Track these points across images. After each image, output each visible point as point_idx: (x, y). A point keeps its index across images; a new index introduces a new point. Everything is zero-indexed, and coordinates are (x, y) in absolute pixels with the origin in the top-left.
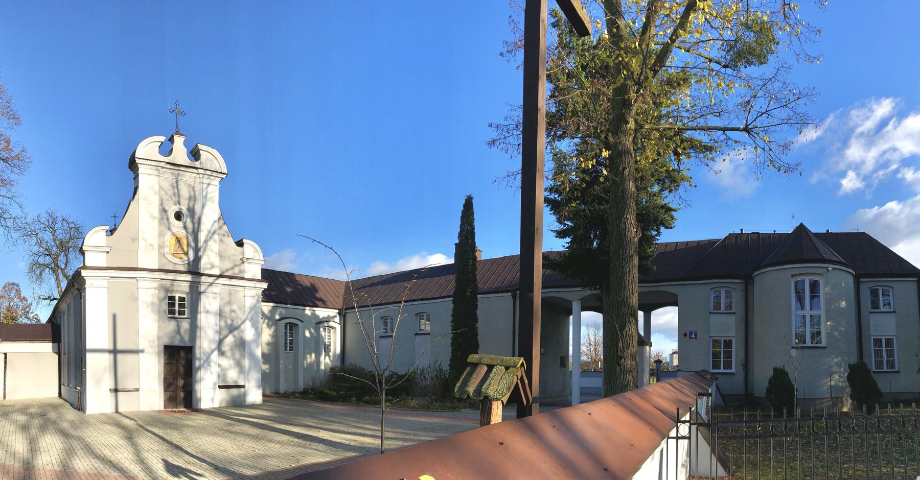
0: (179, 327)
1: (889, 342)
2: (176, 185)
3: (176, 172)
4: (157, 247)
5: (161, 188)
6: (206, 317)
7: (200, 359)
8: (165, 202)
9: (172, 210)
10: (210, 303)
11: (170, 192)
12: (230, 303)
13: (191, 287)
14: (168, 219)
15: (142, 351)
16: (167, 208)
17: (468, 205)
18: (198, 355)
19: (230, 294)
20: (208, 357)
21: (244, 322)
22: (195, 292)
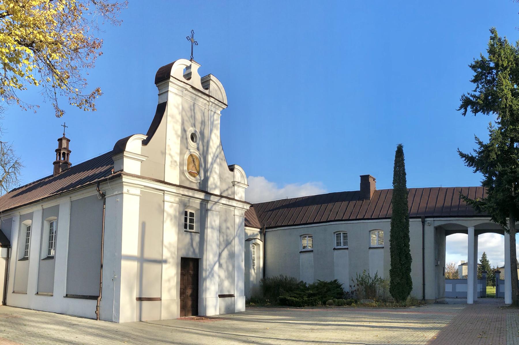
0: (192, 240)
1: (192, 214)
2: (193, 108)
3: (194, 96)
4: (178, 164)
5: (183, 108)
6: (212, 233)
7: (206, 271)
8: (185, 123)
9: (190, 130)
10: (213, 220)
11: (189, 114)
12: (226, 221)
13: (201, 204)
14: (187, 139)
15: (165, 262)
16: (186, 128)
17: (400, 152)
18: (204, 267)
19: (226, 211)
20: (212, 269)
21: (234, 238)
22: (204, 211)
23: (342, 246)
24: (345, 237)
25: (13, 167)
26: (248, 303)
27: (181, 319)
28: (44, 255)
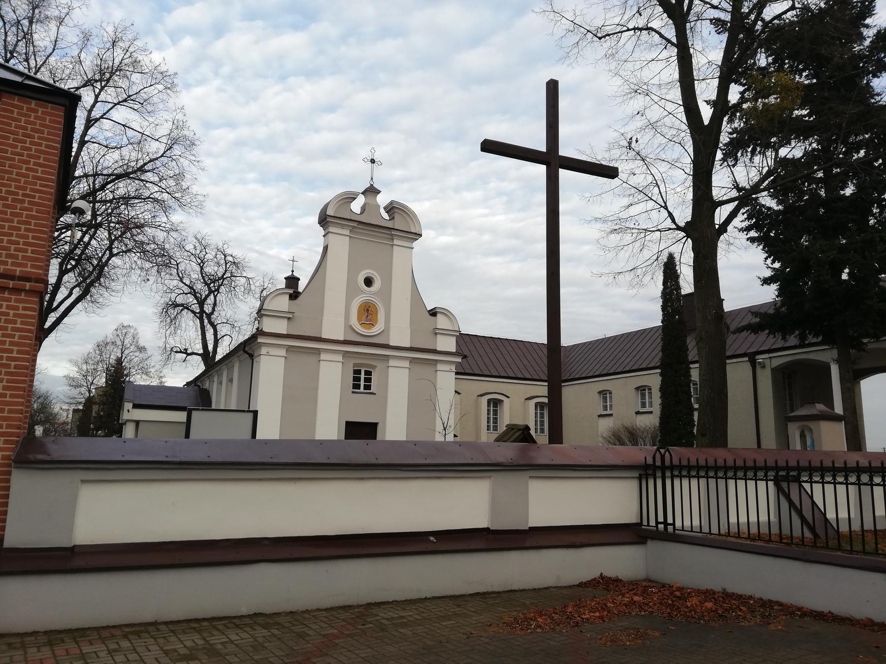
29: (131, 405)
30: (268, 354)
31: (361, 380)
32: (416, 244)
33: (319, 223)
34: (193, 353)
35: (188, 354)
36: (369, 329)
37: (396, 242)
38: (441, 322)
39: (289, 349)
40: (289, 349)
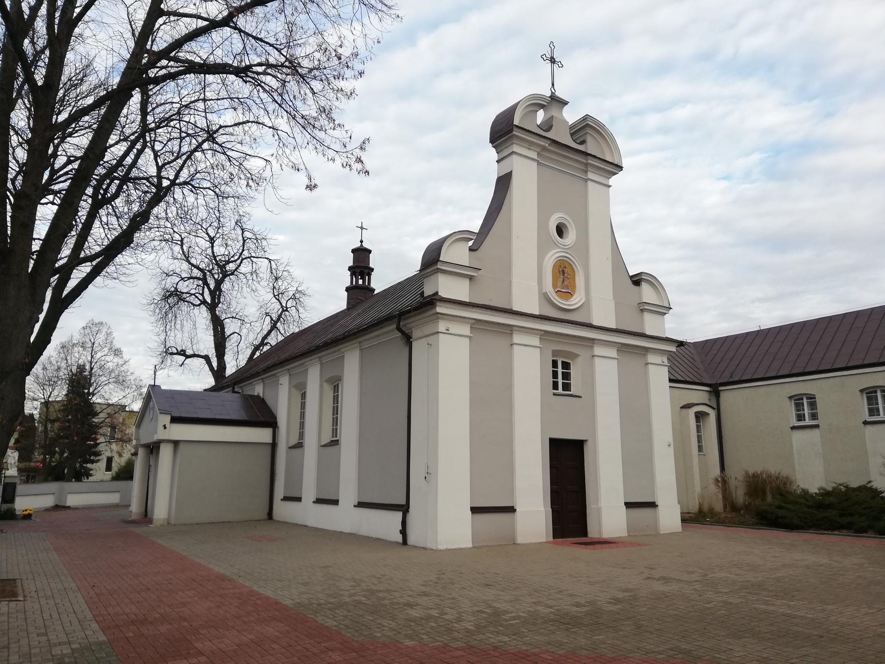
23: (808, 422)
24: (813, 405)
25: (294, 297)
26: (687, 519)
27: (554, 543)
28: (327, 438)
29: (168, 418)
30: (447, 332)
31: (561, 377)
32: (613, 181)
33: (492, 141)
34: (194, 356)
35: (188, 357)
36: (567, 300)
37: (591, 175)
38: (647, 294)
39: (476, 324)
40: (476, 324)
